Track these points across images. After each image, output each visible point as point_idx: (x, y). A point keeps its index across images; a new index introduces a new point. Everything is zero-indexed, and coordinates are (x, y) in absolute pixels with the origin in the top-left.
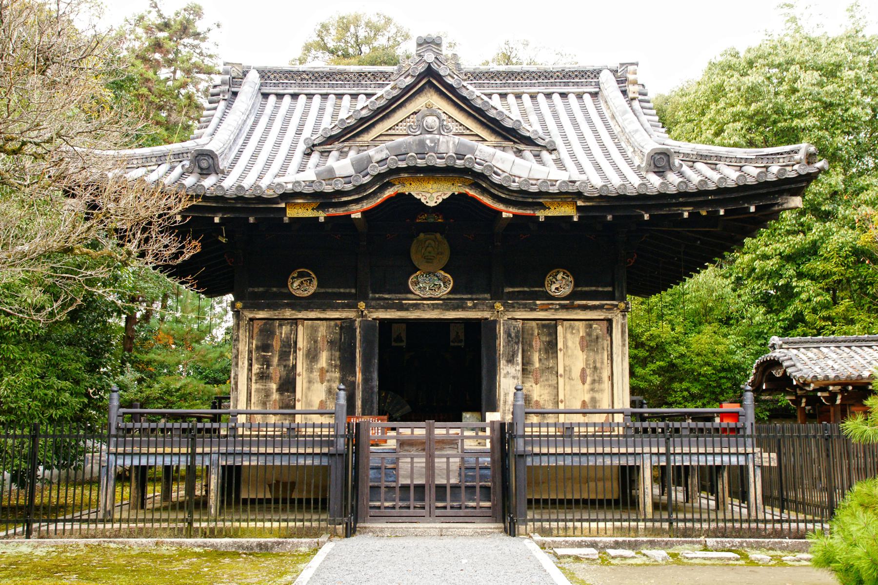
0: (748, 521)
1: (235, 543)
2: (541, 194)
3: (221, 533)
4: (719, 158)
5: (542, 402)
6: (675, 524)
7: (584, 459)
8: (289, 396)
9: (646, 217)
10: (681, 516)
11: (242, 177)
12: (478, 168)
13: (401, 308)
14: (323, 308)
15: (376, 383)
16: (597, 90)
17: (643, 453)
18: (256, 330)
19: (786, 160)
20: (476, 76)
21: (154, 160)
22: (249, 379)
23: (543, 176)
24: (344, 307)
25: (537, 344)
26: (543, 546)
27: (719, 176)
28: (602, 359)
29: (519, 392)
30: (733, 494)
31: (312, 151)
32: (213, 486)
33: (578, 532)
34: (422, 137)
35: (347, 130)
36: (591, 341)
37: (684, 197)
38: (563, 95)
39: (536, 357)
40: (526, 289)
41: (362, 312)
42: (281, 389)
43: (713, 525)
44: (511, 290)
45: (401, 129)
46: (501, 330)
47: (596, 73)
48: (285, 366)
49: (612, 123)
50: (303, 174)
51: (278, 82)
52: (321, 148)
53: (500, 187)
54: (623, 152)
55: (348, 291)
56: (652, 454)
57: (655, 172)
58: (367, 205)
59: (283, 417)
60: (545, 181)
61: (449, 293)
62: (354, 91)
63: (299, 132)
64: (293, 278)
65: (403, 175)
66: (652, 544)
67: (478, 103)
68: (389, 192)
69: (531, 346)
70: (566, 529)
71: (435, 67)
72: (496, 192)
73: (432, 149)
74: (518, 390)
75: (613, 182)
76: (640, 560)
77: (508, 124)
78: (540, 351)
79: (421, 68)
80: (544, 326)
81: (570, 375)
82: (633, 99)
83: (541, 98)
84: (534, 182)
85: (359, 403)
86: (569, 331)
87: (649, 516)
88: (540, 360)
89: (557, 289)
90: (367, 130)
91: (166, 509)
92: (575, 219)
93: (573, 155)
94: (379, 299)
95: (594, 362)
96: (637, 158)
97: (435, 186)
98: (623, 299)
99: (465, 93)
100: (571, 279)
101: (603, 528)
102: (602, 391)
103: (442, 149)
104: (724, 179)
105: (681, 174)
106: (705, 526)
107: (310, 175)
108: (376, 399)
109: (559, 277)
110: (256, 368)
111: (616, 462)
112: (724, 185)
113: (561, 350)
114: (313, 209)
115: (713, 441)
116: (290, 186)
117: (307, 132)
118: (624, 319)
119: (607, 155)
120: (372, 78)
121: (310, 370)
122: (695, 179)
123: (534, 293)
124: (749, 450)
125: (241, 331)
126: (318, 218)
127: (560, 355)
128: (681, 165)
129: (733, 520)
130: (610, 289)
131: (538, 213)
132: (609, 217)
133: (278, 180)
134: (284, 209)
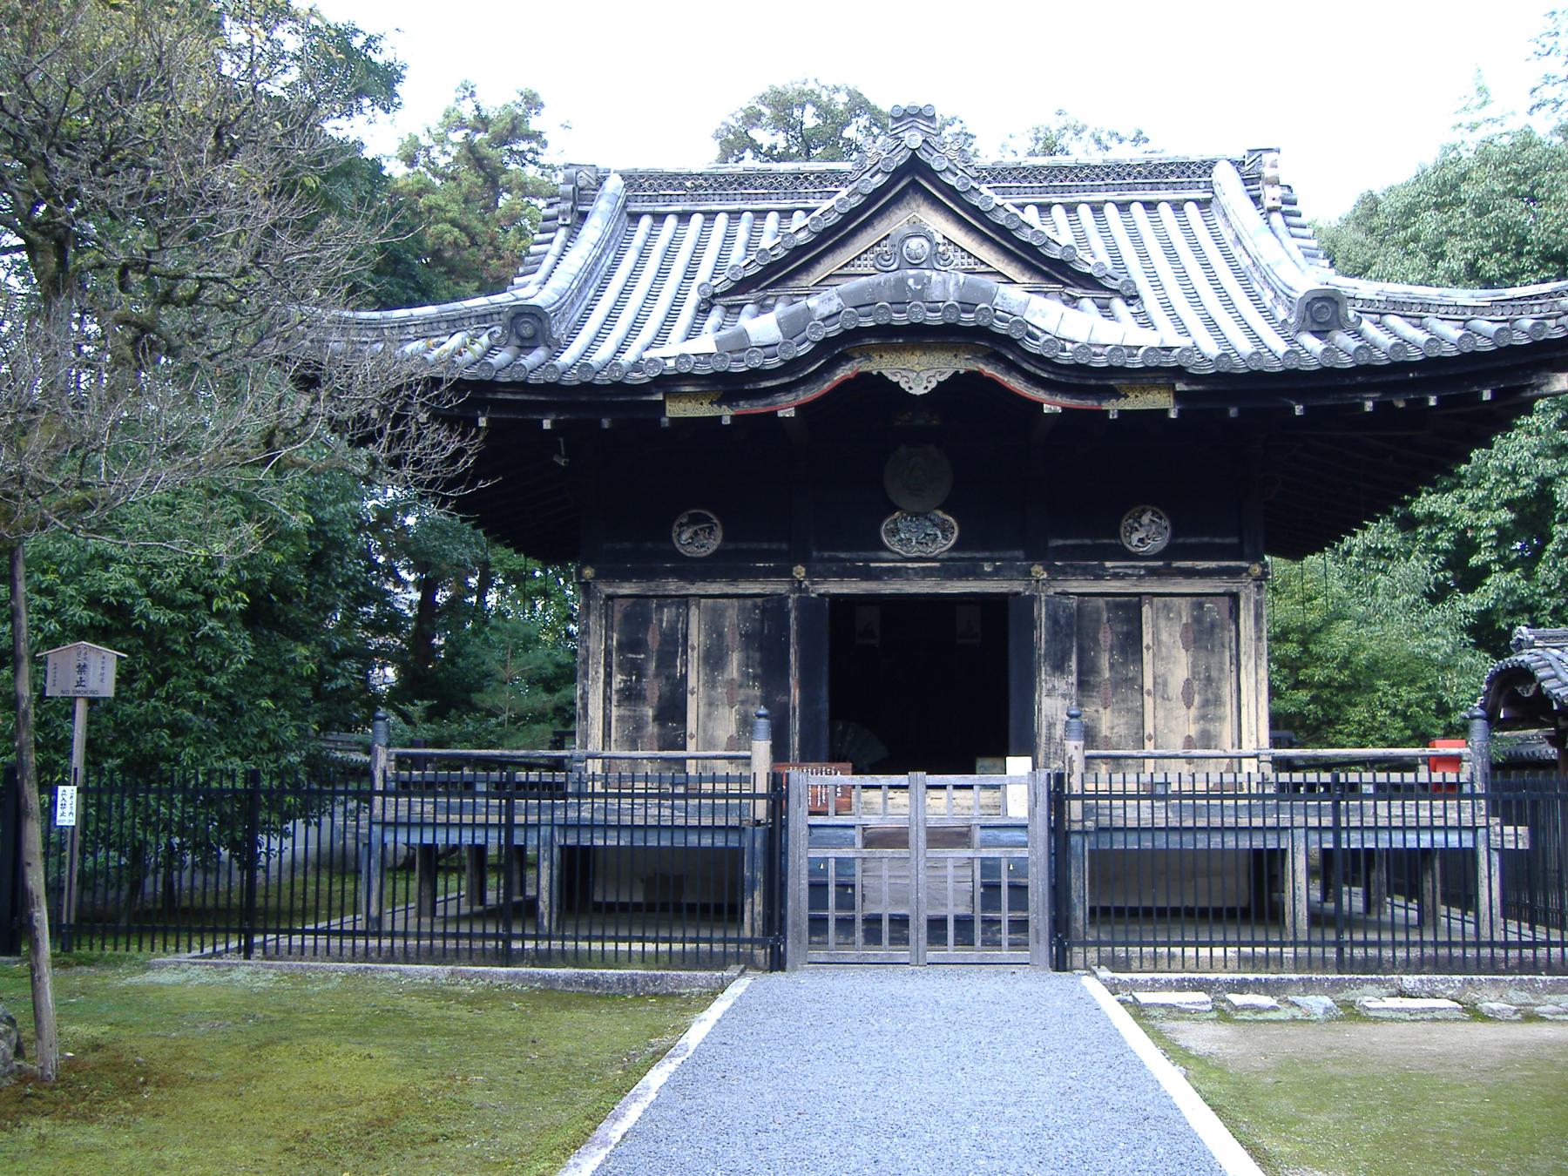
0: (1478, 944)
1: (581, 976)
2: (1111, 371)
3: (564, 958)
4: (1426, 306)
5: (1115, 739)
6: (1347, 950)
7: (1187, 838)
8: (675, 729)
9: (1298, 410)
10: (1359, 937)
11: (589, 350)
12: (1000, 327)
13: (869, 575)
14: (734, 577)
15: (824, 706)
16: (1209, 195)
17: (1292, 828)
18: (618, 616)
19: (1545, 309)
20: (998, 175)
21: (443, 325)
22: (607, 699)
23: (1115, 340)
24: (767, 574)
25: (1106, 637)
26: (1113, 988)
27: (1427, 337)
28: (1222, 663)
29: (1074, 720)
30: (1449, 900)
31: (712, 305)
32: (544, 882)
33: (1177, 965)
34: (899, 274)
35: (771, 269)
36: (1201, 632)
37: (1367, 374)
38: (1150, 206)
39: (1104, 661)
40: (1088, 541)
41: (800, 582)
42: (660, 718)
43: (1415, 952)
44: (1060, 542)
45: (866, 265)
46: (1041, 613)
47: (1208, 166)
48: (668, 678)
49: (1237, 252)
50: (694, 344)
51: (653, 195)
52: (726, 301)
53: (1040, 359)
54: (1255, 299)
55: (774, 546)
56: (1308, 829)
57: (1313, 332)
58: (805, 395)
59: (666, 765)
60: (1118, 348)
61: (950, 550)
62: (786, 204)
63: (689, 274)
64: (681, 525)
65: (867, 341)
66: (1308, 987)
67: (1000, 219)
68: (844, 372)
69: (1096, 642)
70: (1155, 958)
71: (923, 156)
72: (1032, 369)
73: (919, 295)
74: (1071, 716)
75: (1240, 349)
76: (1283, 1014)
77: (1055, 253)
78: (1111, 650)
79: (900, 159)
80: (1118, 606)
81: (1165, 691)
82: (1271, 210)
83: (1110, 211)
84: (1099, 350)
85: (795, 741)
86: (1162, 615)
87: (1303, 937)
88: (1112, 666)
89: (1141, 540)
90: (807, 267)
91: (471, 918)
92: (1173, 415)
93: (1167, 306)
94: (830, 560)
95: (1208, 669)
96: (1280, 308)
97: (925, 359)
98: (1257, 558)
99: (976, 201)
100: (1166, 523)
101: (1217, 957)
102: (1221, 719)
103: (936, 293)
104: (1437, 339)
105: (1358, 334)
106: (1401, 953)
107: (706, 343)
108: (825, 735)
109: (1146, 519)
110: (618, 680)
111: (1244, 843)
112: (1436, 353)
113: (1148, 648)
114: (711, 403)
115: (1459, 806)
116: (671, 363)
117: (703, 274)
118: (1259, 593)
119: (1228, 304)
120: (817, 182)
121: (711, 683)
122: (1385, 340)
123: (1097, 543)
124: (1481, 821)
125: (592, 617)
126: (720, 418)
127: (1147, 656)
128: (1360, 319)
129: (1450, 944)
130: (1234, 540)
131: (1105, 406)
132: (1233, 412)
133: (647, 355)
134: (662, 404)
